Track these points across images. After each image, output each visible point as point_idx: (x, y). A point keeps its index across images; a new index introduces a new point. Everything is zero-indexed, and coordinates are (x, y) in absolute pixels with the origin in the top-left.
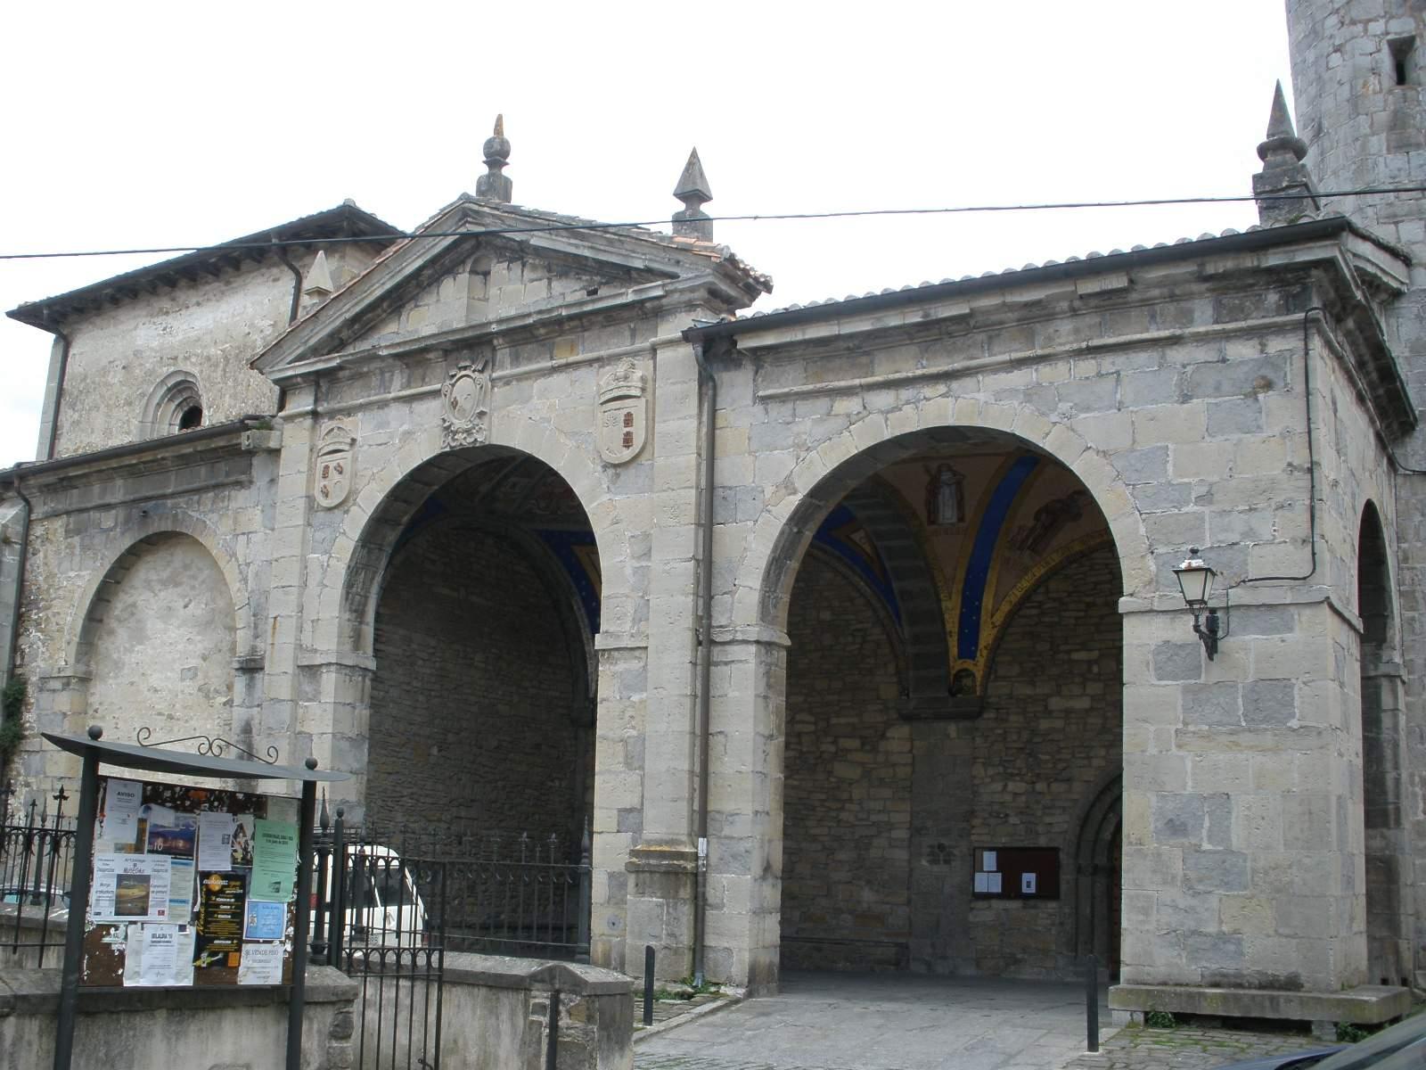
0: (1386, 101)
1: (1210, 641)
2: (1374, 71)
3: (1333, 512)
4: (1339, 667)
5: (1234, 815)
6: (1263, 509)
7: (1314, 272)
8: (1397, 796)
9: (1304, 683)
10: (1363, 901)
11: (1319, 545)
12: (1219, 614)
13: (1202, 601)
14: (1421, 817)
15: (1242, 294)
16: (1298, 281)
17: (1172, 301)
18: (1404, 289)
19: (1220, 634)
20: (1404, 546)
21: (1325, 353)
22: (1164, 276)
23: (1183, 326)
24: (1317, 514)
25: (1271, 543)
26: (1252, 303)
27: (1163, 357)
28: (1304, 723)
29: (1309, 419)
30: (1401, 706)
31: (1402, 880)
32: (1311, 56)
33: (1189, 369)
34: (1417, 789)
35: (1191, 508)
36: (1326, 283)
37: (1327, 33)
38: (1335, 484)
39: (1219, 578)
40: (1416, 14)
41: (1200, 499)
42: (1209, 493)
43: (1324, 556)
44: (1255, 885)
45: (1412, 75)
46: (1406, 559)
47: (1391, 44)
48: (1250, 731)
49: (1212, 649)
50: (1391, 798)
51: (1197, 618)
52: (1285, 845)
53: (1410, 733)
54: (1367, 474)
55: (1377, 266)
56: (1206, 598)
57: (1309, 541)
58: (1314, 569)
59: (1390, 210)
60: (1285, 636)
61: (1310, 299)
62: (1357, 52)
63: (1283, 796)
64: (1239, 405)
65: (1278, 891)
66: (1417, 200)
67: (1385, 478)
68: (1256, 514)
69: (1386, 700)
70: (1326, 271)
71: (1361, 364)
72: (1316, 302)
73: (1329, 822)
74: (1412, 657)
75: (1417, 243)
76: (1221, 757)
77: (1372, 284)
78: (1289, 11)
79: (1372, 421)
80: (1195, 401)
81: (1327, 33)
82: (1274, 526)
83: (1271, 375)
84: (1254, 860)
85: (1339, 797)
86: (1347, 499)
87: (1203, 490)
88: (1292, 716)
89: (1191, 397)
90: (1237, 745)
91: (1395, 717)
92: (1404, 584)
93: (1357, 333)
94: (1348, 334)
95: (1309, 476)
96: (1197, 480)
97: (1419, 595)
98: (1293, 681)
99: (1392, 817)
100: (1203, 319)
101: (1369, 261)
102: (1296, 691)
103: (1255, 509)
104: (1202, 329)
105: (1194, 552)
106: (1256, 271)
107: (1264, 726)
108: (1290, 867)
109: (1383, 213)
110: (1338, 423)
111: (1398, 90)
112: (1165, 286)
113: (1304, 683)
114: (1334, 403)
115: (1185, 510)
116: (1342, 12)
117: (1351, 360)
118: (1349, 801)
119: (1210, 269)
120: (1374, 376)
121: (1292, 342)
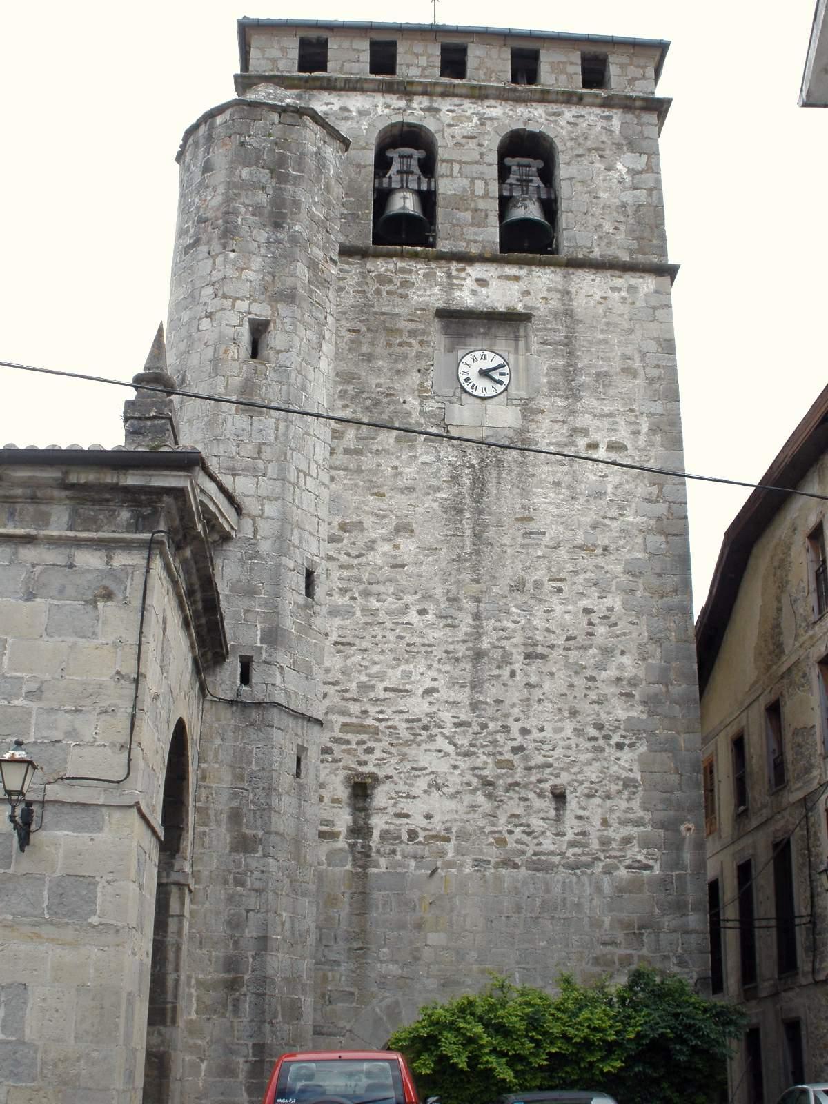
0: (241, 369)
1: (23, 833)
2: (235, 341)
3: (150, 723)
4: (139, 871)
5: (29, 1005)
6: (87, 711)
7: (166, 499)
8: (176, 997)
9: (108, 882)
10: (140, 1094)
11: (136, 752)
12: (35, 808)
13: (21, 793)
14: (194, 1016)
15: (97, 507)
16: (149, 503)
17: (32, 502)
18: (233, 534)
19: (33, 827)
20: (204, 765)
21: (163, 574)
22: (30, 478)
23: (38, 527)
24: (137, 723)
25: (92, 745)
26: (105, 517)
27: (15, 554)
28: (103, 921)
29: (141, 633)
30: (187, 913)
31: (173, 1074)
32: (186, 316)
33: (38, 569)
34: (193, 991)
35: (20, 702)
36: (174, 511)
37: (203, 300)
38: (156, 697)
39: (39, 772)
40: (273, 303)
41: (29, 695)
42: (40, 690)
43: (139, 763)
44: (44, 1077)
45: (264, 352)
46: (204, 778)
47: (251, 322)
48: (52, 924)
49: (24, 841)
50: (170, 998)
51: (14, 808)
52: (75, 1038)
53: (191, 938)
54: (182, 694)
55: (217, 507)
56: (24, 790)
57: (127, 747)
58: (129, 774)
59: (230, 464)
60: (94, 835)
61: (158, 522)
62: (224, 322)
63: (77, 990)
64: (79, 610)
65: (66, 1084)
66: (253, 458)
67: (195, 701)
68: (81, 715)
69: (174, 907)
70: (176, 498)
71: (190, 593)
72: (162, 526)
73: (118, 1017)
74: (199, 868)
75: (248, 496)
76: (23, 947)
77: (211, 521)
78: (174, 274)
79: (192, 647)
80: (38, 600)
81: (203, 300)
82: (96, 728)
83: (113, 586)
84: (45, 1052)
85: (129, 994)
86: (164, 713)
87: (34, 686)
88: (94, 912)
89: (35, 596)
90: (39, 936)
91: (181, 922)
92: (200, 801)
93: (192, 563)
94: (184, 562)
95: (134, 686)
96: (30, 675)
97: (211, 812)
98: (98, 879)
99: (169, 1015)
100: (58, 524)
101: (212, 499)
102: (99, 889)
103: (81, 711)
104: (55, 533)
105: (19, 744)
106: (115, 488)
107: (66, 920)
108: (78, 1060)
109: (225, 465)
110: (165, 641)
111: (251, 362)
112: (29, 487)
113: (108, 882)
114: (164, 622)
115: (15, 702)
116: (217, 286)
117: (183, 586)
118: (138, 998)
119: (73, 478)
120: (200, 606)
121: (135, 559)
